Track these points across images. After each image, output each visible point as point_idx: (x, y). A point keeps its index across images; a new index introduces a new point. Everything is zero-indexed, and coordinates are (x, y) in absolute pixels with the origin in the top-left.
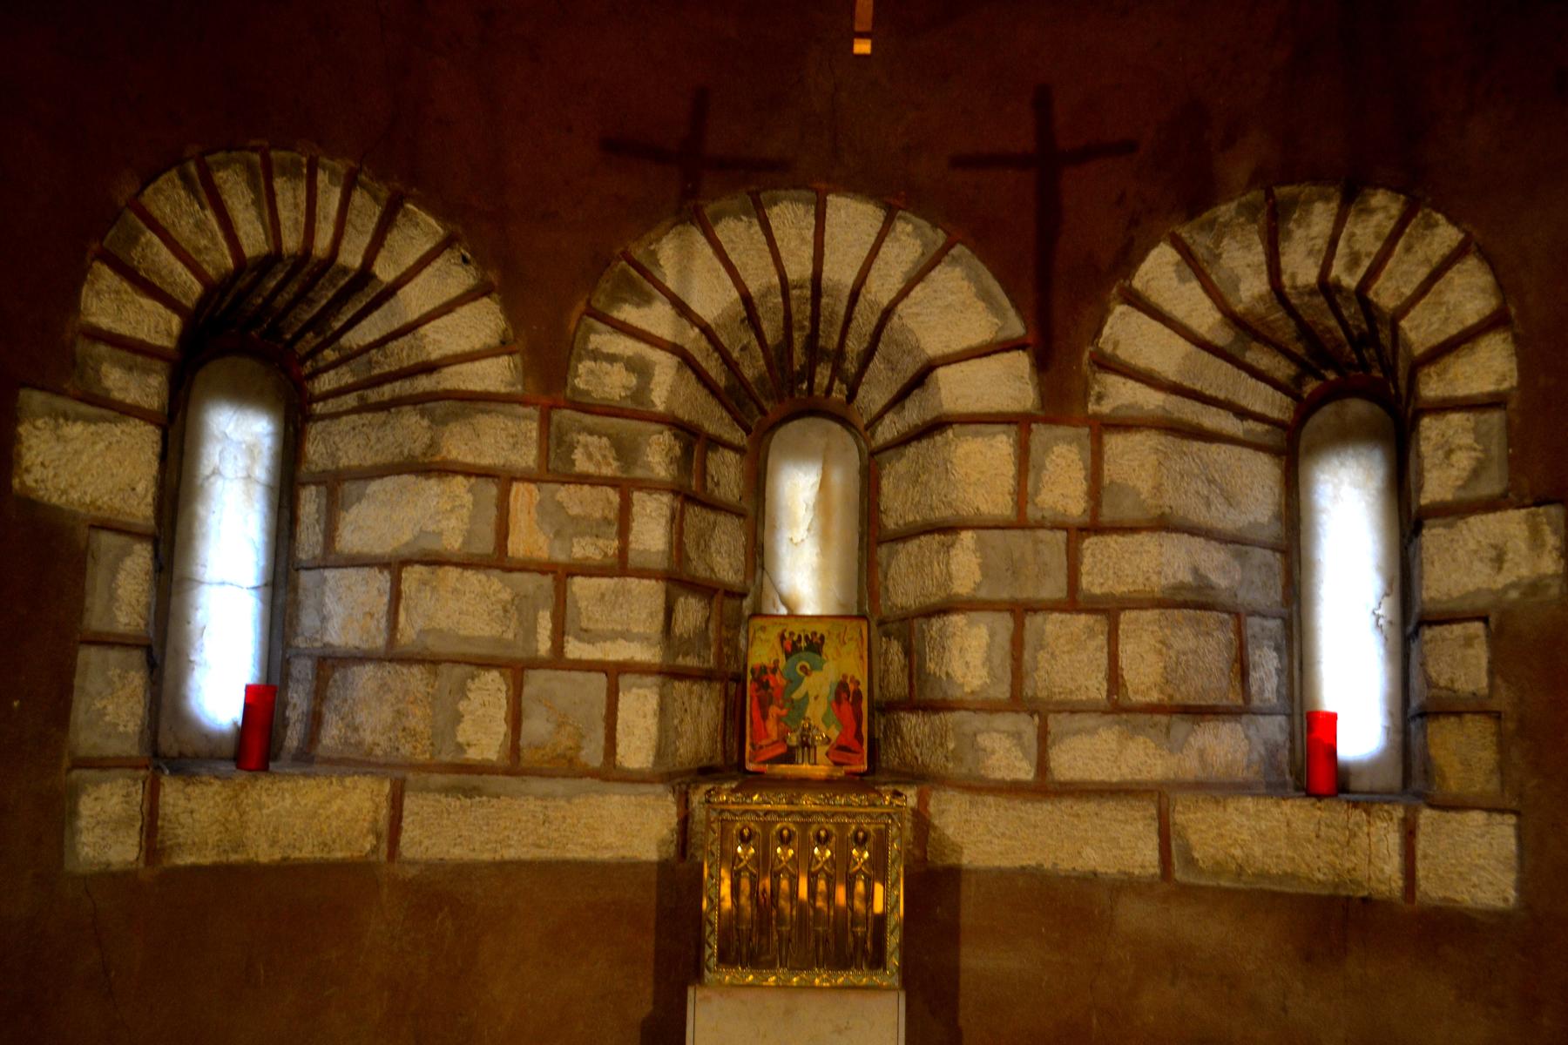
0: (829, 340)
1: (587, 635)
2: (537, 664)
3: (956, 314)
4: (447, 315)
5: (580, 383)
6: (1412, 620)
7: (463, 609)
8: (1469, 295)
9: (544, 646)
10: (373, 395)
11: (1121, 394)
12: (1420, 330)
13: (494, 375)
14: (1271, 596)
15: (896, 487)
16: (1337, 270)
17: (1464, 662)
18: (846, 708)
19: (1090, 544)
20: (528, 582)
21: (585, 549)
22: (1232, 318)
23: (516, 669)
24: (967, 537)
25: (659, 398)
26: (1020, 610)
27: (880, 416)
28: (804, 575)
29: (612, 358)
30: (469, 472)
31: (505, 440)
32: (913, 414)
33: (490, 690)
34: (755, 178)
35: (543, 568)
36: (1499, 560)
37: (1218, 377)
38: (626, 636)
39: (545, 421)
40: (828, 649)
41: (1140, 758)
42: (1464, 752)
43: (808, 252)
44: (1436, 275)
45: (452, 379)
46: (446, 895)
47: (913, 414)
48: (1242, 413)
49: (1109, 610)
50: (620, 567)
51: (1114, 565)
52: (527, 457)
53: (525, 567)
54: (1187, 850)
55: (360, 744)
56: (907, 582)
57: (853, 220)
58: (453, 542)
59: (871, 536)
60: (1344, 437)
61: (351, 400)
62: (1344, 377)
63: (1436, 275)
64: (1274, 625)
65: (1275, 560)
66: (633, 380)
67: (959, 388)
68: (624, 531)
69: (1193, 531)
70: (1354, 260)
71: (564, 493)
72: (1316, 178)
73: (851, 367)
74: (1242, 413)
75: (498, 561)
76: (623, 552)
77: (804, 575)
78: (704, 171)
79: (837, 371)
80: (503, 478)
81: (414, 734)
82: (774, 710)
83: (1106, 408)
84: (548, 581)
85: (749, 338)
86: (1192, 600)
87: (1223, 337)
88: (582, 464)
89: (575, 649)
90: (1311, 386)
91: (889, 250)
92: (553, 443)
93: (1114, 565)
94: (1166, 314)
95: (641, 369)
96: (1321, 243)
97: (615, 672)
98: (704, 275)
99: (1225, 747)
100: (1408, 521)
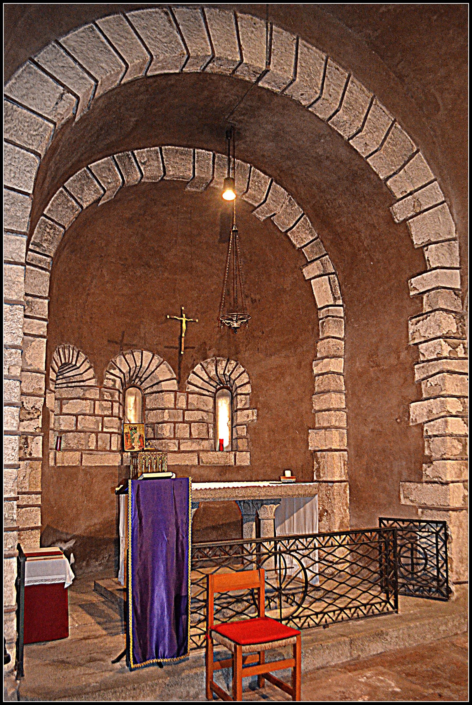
0: (140, 375)
1: (107, 428)
2: (100, 432)
3: (165, 372)
4: (85, 371)
5: (105, 383)
6: (233, 425)
7: (88, 423)
8: (245, 378)
9: (100, 429)
10: (70, 385)
11: (192, 388)
12: (238, 383)
13: (92, 382)
14: (212, 421)
15: (150, 401)
16: (226, 372)
17: (242, 431)
18: (141, 440)
19: (186, 412)
20: (98, 418)
21: (106, 413)
22: (209, 377)
23: (97, 433)
24: (167, 411)
25: (117, 387)
26: (175, 423)
27: (147, 388)
28: (132, 416)
29: (110, 379)
30: (90, 399)
31: (94, 394)
32: (155, 389)
33: (195, 435)
34: (132, 347)
35: (100, 416)
36: (248, 417)
37: (206, 386)
38: (113, 427)
39: (100, 390)
40: (138, 429)
41: (195, 447)
42: (242, 444)
43: (140, 361)
44: (240, 375)
45: (87, 383)
46: (88, 471)
47: (155, 389)
48: (209, 391)
49: (190, 423)
50: (112, 416)
51: (189, 416)
52: (98, 397)
53: (98, 416)
54: (202, 460)
55: (70, 447)
56: (152, 417)
57: (147, 355)
58: (88, 412)
59: (144, 409)
60: (223, 395)
61: (65, 385)
62: (225, 386)
63: (240, 375)
64: (212, 425)
65: (212, 415)
66: (113, 383)
67: (165, 386)
68: (112, 410)
69: (202, 410)
70: (229, 371)
71: (103, 403)
72: (223, 356)
73: (142, 379)
74: (209, 391)
75: (94, 415)
76: (112, 413)
77: (132, 416)
78: (123, 345)
79: (140, 380)
80: (94, 400)
81: (82, 445)
82: (129, 440)
83: (189, 390)
84: (101, 418)
85: (128, 375)
86: (202, 421)
87: (207, 380)
88: (106, 398)
89: (105, 430)
90: (218, 387)
91: (153, 361)
92: (101, 394)
93: (189, 416)
94: (199, 376)
95: (114, 381)
96: (224, 368)
97: (111, 433)
98: (123, 365)
99: (206, 444)
100: (233, 411)
